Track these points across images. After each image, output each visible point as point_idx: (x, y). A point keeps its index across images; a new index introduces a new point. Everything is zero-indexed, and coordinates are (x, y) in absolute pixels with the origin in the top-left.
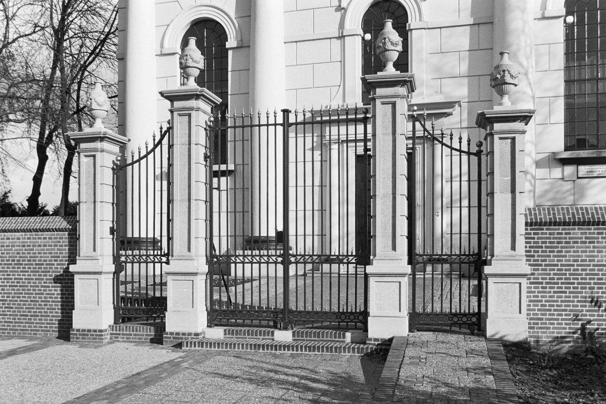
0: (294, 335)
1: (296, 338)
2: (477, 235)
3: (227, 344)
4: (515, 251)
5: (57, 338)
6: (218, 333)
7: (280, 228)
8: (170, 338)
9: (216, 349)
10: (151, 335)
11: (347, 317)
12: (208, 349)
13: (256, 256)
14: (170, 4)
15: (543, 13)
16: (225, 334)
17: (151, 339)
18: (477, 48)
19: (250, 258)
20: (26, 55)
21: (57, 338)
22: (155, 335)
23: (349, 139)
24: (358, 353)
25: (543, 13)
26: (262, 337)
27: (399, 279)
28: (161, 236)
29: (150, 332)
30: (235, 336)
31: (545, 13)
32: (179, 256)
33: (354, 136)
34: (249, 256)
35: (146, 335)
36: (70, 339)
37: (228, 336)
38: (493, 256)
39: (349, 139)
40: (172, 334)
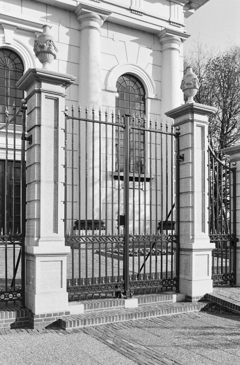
0: (139, 302)
1: (141, 304)
2: (111, 221)
3: (145, 313)
4: (57, 233)
5: (13, 326)
6: (78, 309)
7: (122, 213)
8: (41, 320)
9: (73, 327)
10: (11, 321)
11: (15, 296)
12: (91, 325)
13: (83, 236)
14: (60, 67)
15: (106, 88)
16: (85, 309)
17: (12, 325)
18: (69, 99)
19: (84, 239)
20: (217, 107)
21: (13, 326)
22: (16, 320)
23: (8, 148)
24: (197, 309)
25: (106, 88)
26: (116, 307)
27: (61, 258)
28: (106, 220)
29: (10, 317)
30: (103, 308)
31: (107, 87)
32: (46, 237)
33: (13, 146)
34: (84, 236)
35: (6, 321)
36: (33, 325)
37: (87, 310)
38: (40, 237)
39: (16, 148)
40: (43, 316)
